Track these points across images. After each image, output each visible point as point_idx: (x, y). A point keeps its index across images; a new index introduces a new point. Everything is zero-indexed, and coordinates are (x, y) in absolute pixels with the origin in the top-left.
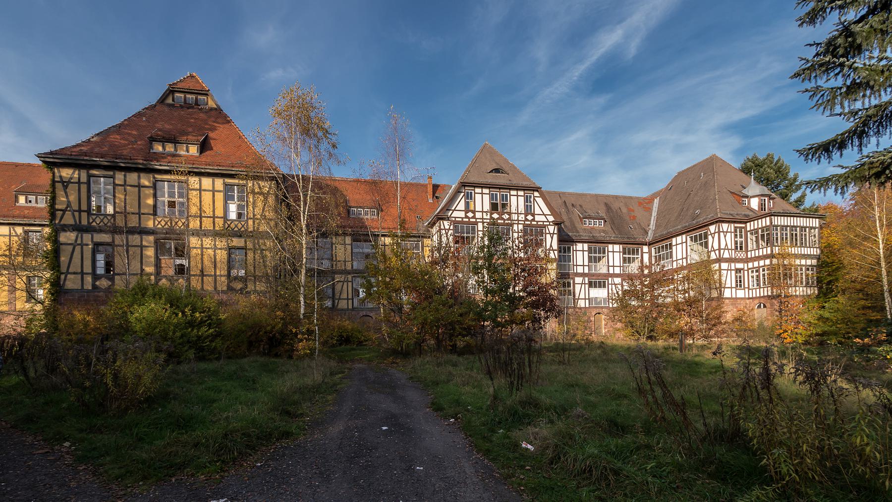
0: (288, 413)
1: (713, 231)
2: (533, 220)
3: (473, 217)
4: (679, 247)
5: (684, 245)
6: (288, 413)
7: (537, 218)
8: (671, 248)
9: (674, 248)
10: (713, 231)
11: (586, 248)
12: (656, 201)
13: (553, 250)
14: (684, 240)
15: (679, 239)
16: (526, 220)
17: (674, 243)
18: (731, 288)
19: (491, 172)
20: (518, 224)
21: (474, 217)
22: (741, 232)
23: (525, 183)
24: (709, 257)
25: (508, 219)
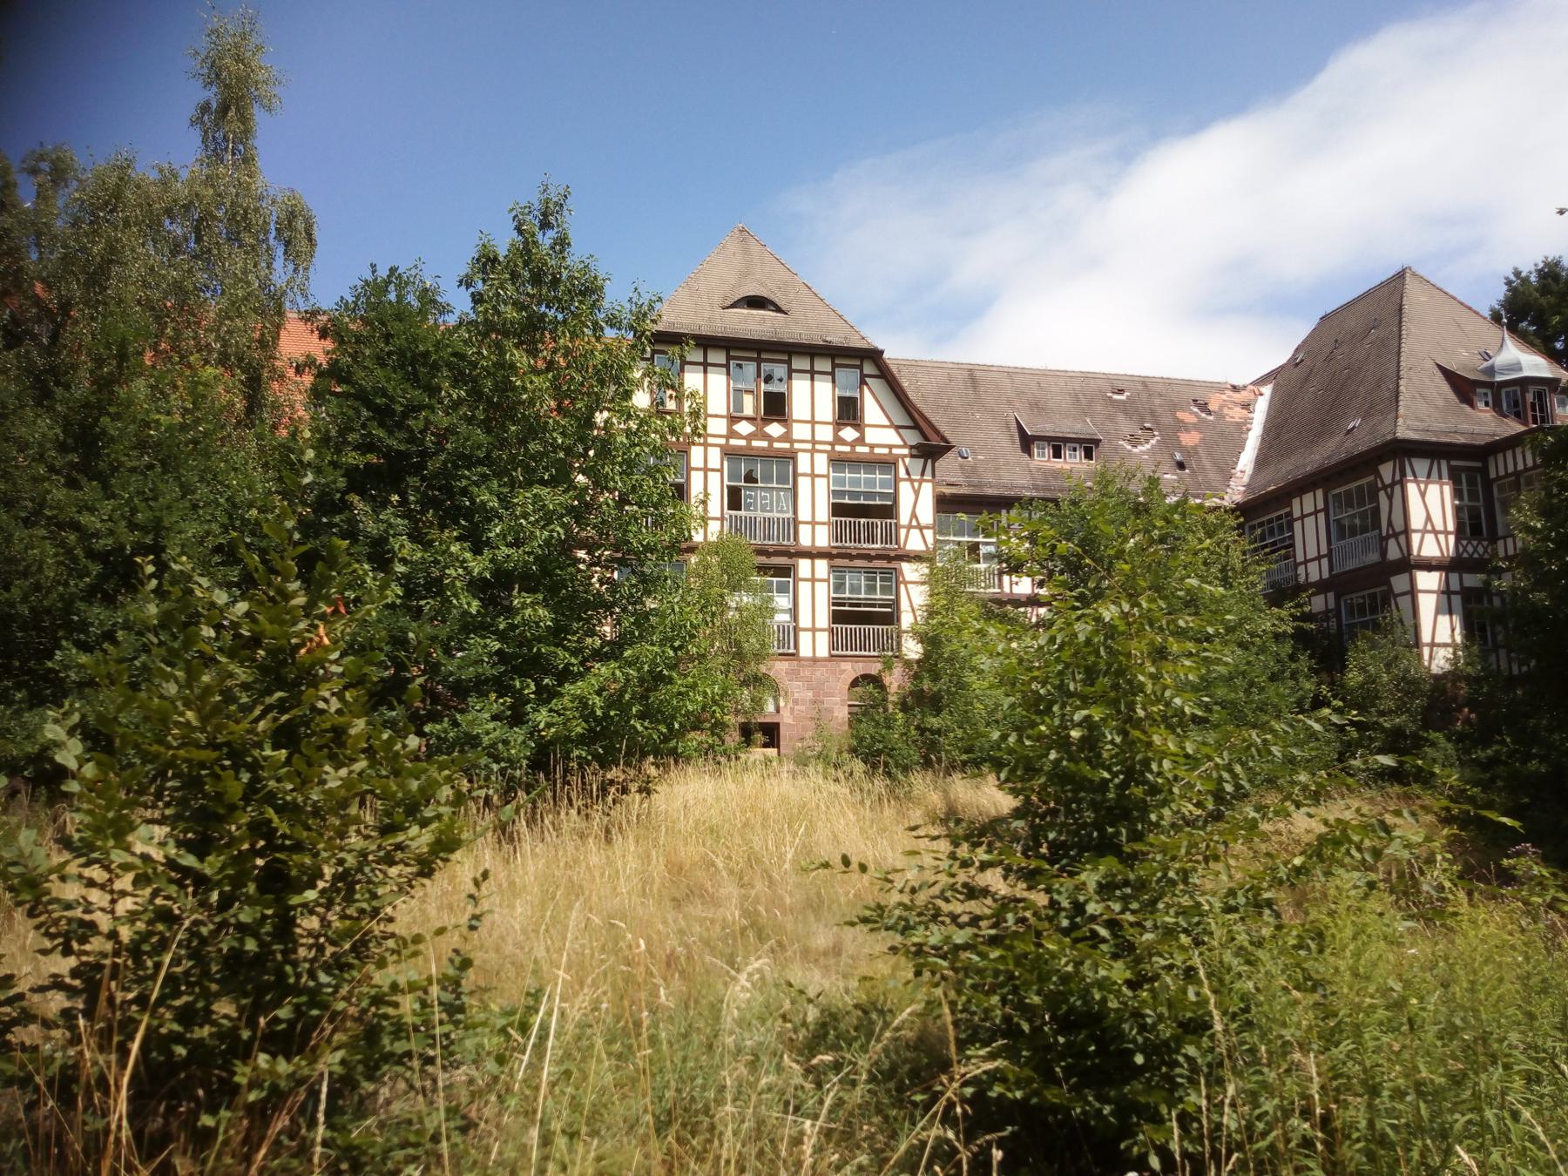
0: (608, 831)
1: (1388, 480)
2: (861, 441)
3: (781, 439)
4: (1310, 521)
5: (1321, 516)
6: (608, 831)
7: (872, 436)
8: (1291, 528)
9: (1297, 525)
10: (1388, 480)
11: (805, 532)
12: (1267, 390)
13: (921, 528)
14: (1321, 505)
15: (1308, 499)
16: (839, 440)
17: (1297, 514)
18: (1433, 645)
19: (733, 306)
20: (813, 451)
21: (787, 437)
22: (1471, 482)
23: (836, 339)
24: (1384, 552)
25: (781, 439)
